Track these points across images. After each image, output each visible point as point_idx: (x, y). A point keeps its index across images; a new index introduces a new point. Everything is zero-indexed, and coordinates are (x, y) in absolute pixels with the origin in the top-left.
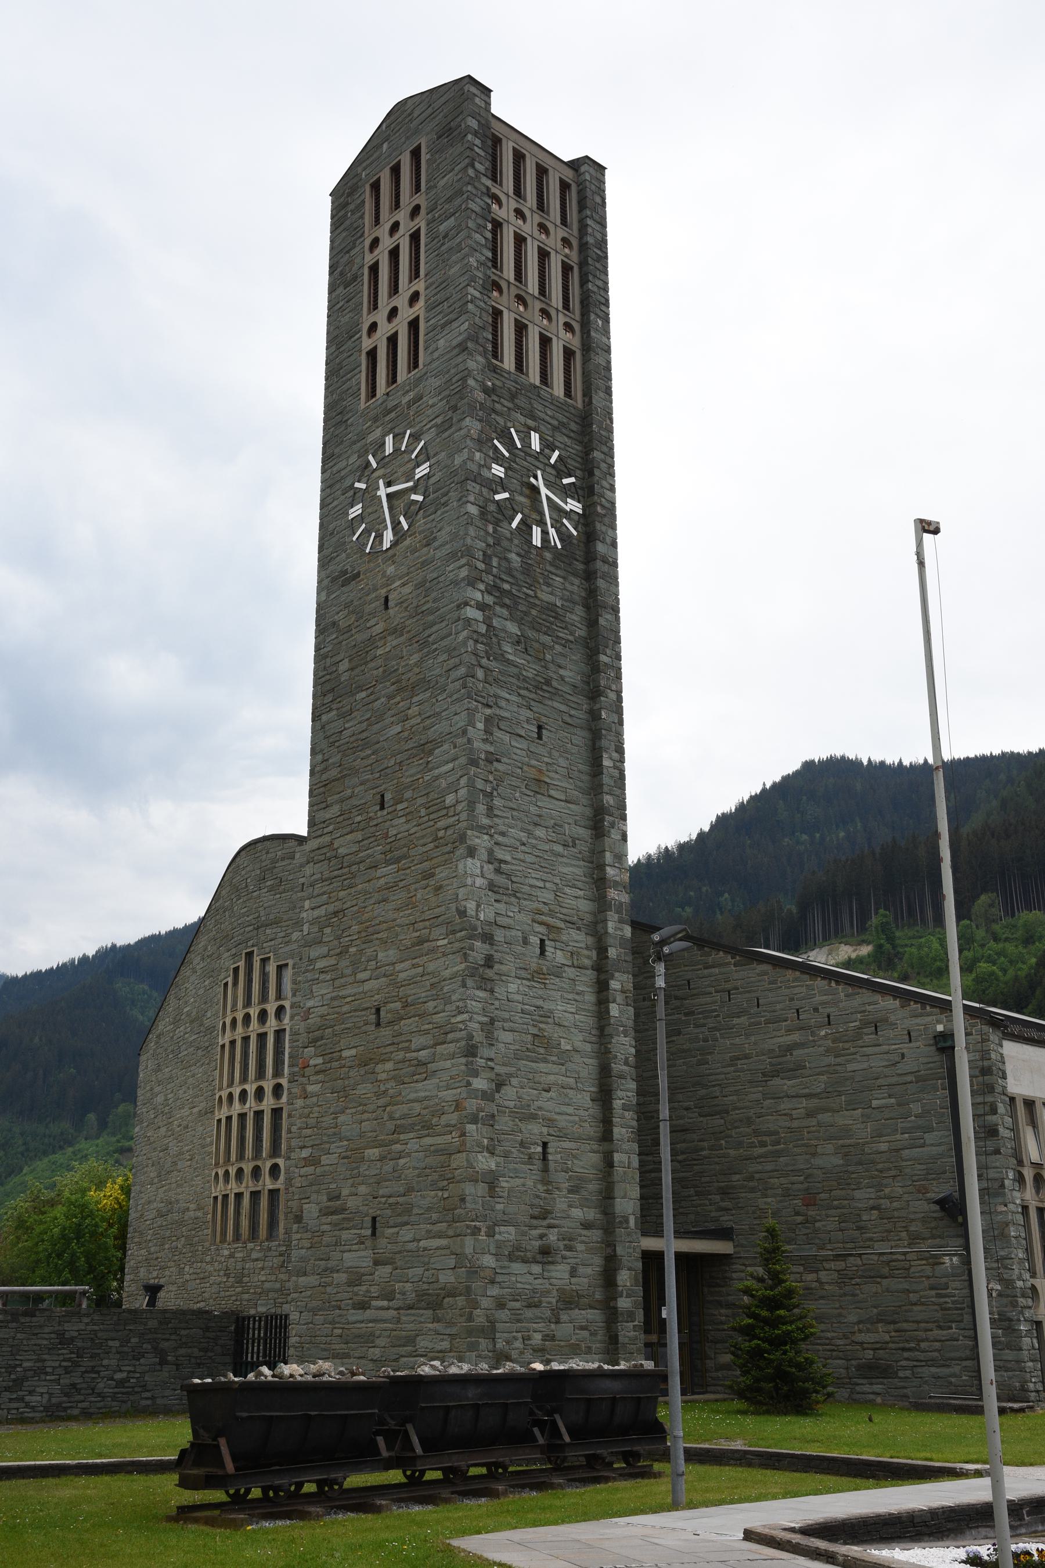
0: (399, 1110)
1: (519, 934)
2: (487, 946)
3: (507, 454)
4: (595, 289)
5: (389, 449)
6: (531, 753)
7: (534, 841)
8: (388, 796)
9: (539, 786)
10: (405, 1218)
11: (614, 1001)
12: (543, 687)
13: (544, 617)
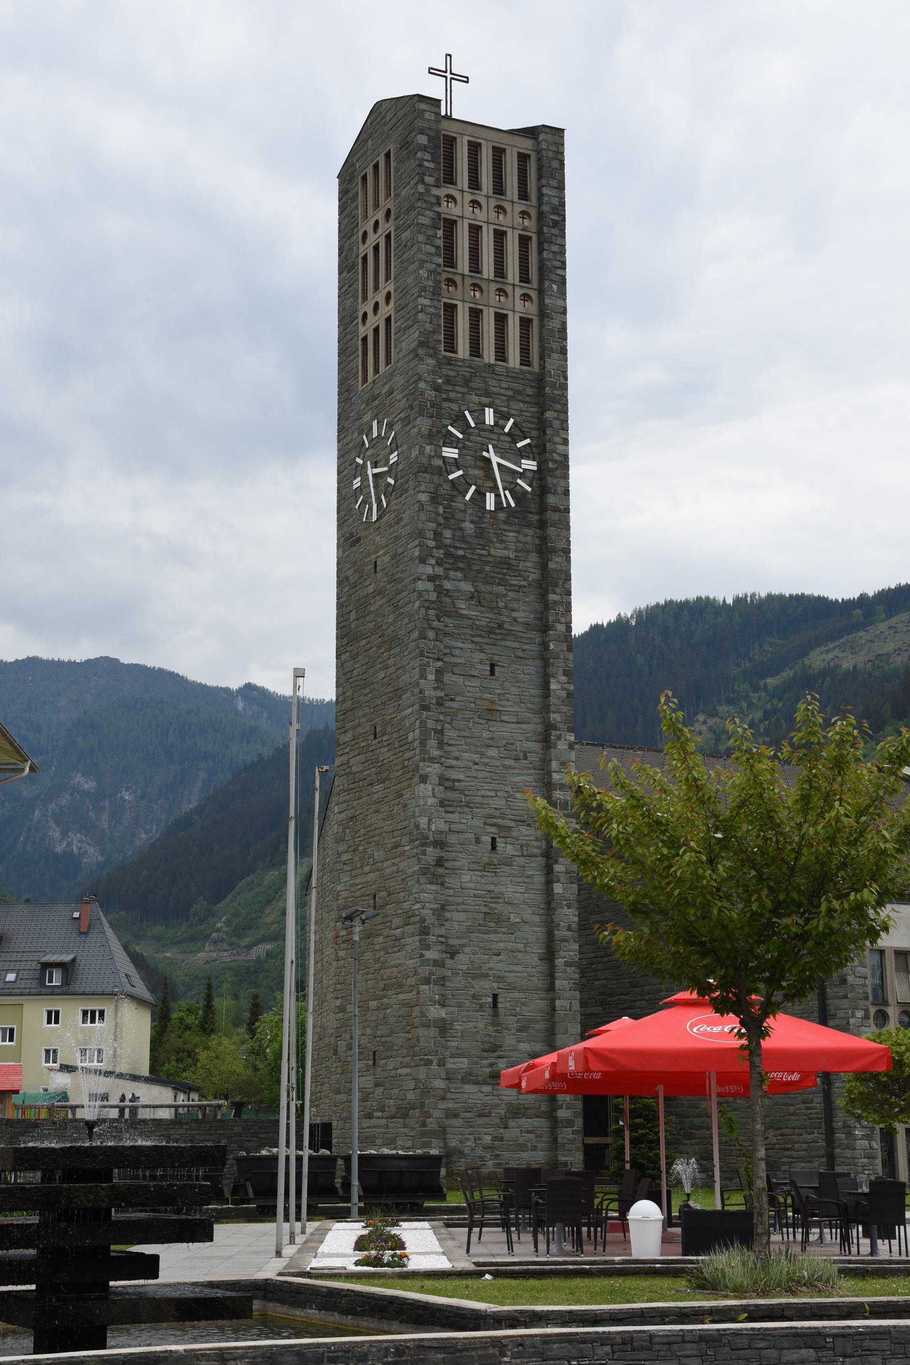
0: (386, 973)
1: (472, 836)
2: (438, 850)
3: (461, 436)
4: (551, 256)
6: (483, 689)
7: (486, 760)
8: (378, 729)
9: (491, 714)
10: (389, 1053)
11: (558, 881)
12: (496, 631)
13: (497, 570)
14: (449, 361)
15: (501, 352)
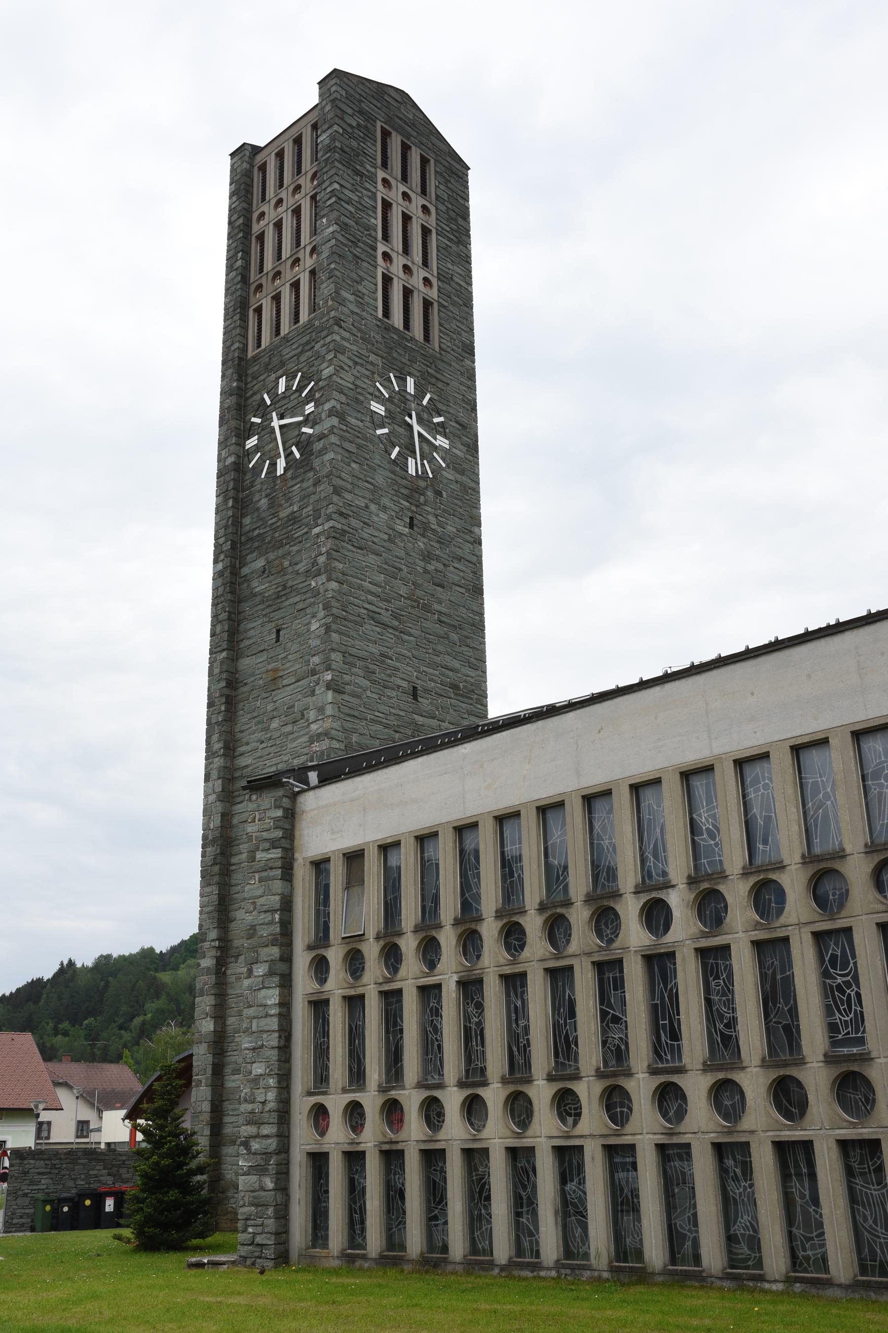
5: (282, 388)
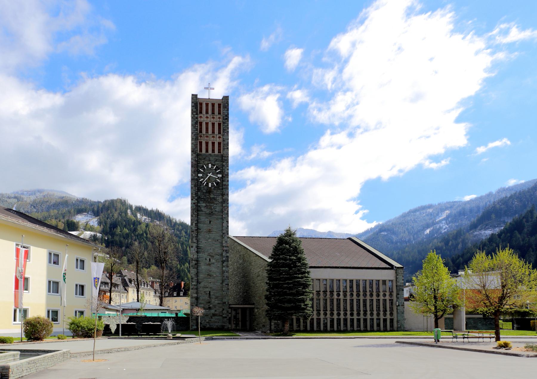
9: (210, 231)
14: (200, 154)
15: (213, 151)
